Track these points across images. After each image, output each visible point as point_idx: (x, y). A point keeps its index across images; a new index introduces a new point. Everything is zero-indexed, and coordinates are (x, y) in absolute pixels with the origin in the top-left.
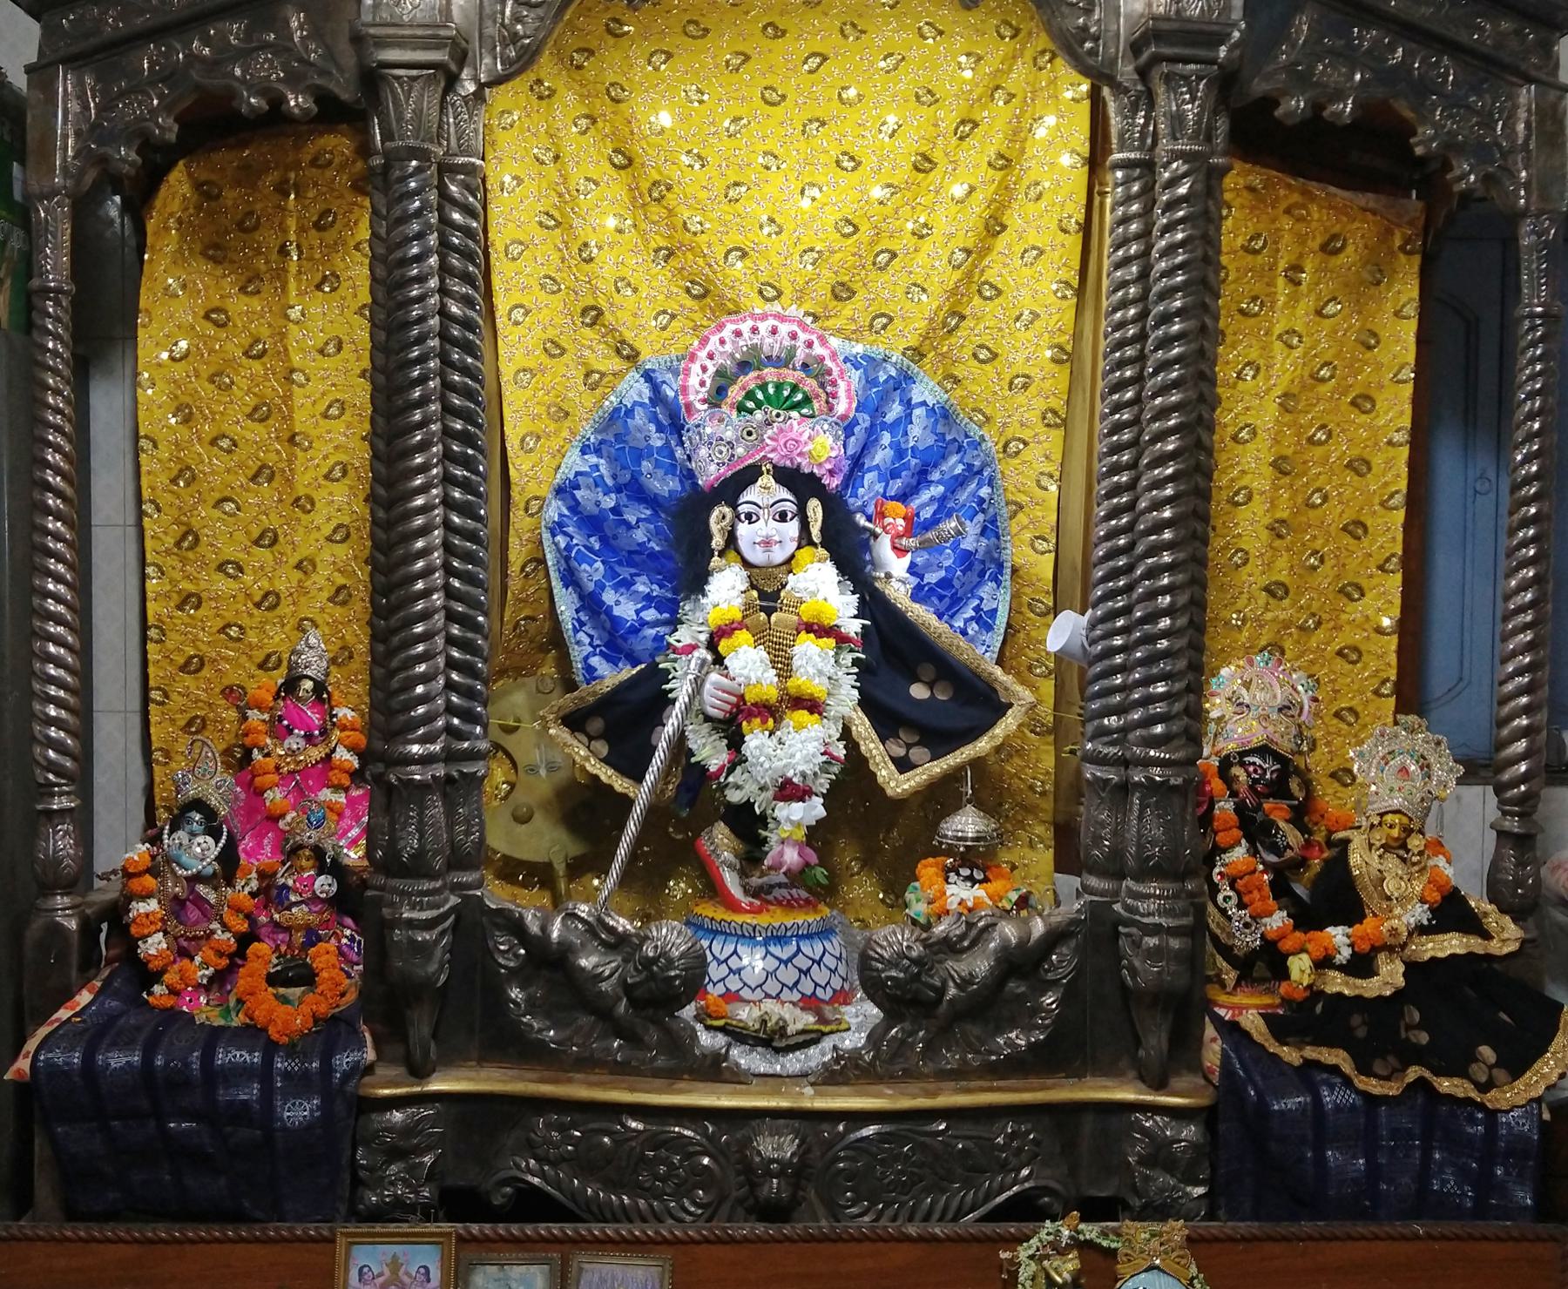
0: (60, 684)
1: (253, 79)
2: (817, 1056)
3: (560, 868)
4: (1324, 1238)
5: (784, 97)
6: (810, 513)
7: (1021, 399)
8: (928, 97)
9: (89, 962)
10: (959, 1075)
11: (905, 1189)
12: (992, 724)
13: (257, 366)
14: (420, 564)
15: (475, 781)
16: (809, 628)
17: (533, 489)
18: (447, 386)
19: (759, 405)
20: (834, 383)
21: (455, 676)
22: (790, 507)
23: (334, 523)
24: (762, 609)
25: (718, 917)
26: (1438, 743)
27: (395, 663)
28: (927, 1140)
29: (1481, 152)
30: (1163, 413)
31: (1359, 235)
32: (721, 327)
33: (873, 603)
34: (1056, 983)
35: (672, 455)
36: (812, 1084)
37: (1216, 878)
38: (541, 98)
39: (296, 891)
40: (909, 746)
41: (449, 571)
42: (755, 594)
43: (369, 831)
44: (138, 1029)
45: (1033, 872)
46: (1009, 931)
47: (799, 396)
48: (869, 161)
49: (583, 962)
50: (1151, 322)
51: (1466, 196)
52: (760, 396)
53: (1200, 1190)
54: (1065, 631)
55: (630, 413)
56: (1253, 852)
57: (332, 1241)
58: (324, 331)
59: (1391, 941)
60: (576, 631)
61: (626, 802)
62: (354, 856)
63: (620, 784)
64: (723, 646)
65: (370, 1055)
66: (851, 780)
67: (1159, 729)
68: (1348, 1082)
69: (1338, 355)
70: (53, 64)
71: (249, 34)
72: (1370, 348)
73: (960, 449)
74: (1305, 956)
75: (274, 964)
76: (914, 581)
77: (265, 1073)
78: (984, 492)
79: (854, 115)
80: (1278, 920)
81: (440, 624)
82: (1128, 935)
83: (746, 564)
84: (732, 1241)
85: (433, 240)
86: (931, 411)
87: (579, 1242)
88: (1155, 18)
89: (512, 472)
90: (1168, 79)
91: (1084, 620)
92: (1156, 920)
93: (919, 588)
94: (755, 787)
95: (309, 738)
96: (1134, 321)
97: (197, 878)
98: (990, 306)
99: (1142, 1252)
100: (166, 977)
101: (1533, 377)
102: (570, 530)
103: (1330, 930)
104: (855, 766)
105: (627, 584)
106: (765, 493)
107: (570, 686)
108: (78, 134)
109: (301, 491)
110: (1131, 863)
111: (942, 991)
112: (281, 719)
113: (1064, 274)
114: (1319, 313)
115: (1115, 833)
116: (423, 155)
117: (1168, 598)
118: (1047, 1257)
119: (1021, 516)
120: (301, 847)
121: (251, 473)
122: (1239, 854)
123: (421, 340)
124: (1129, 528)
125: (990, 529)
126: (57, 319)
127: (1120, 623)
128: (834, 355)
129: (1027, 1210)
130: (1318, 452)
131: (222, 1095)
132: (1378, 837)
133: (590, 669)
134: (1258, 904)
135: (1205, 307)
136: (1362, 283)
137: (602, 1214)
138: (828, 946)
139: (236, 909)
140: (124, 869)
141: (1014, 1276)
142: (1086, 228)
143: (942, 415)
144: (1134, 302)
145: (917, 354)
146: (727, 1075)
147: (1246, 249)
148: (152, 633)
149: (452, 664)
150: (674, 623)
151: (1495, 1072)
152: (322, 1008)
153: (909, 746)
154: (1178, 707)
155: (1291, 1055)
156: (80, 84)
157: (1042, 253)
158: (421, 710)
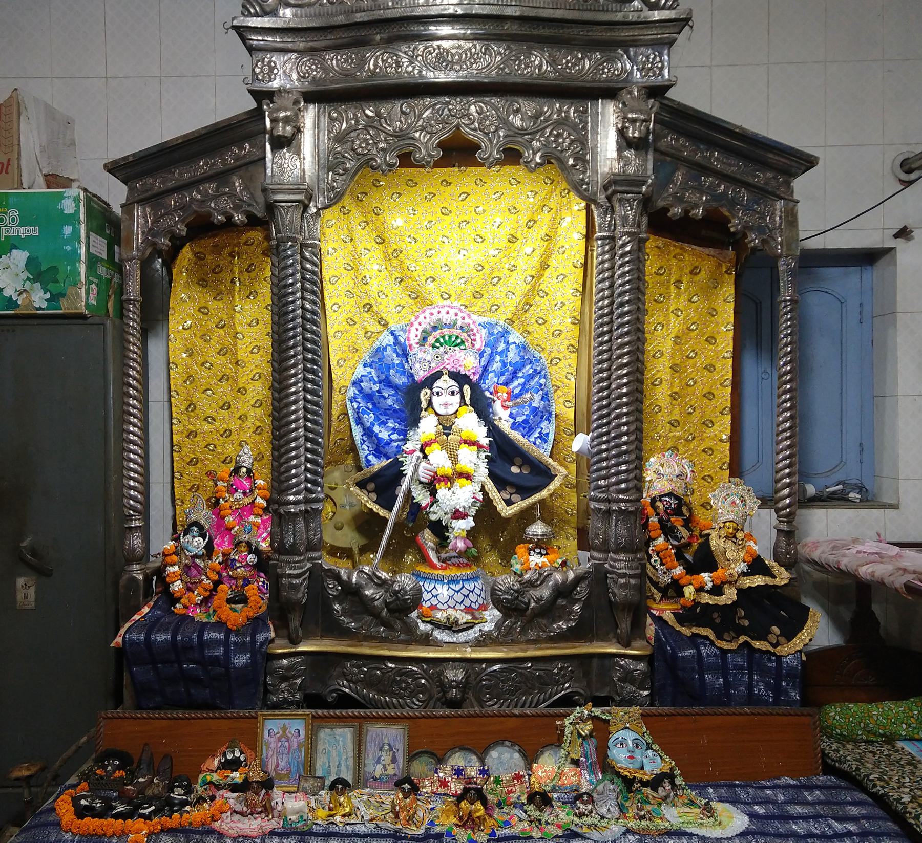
0: (135, 472)
2: (472, 634)
3: (356, 550)
6: (465, 391)
7: (558, 340)
8: (514, 210)
9: (148, 594)
11: (513, 693)
12: (548, 484)
13: (221, 331)
14: (294, 416)
15: (317, 512)
16: (465, 442)
17: (342, 383)
18: (305, 339)
20: (474, 335)
21: (309, 465)
22: (456, 389)
23: (255, 399)
24: (444, 434)
25: (427, 571)
27: (282, 460)
29: (760, 230)
30: (622, 346)
31: (707, 266)
32: (424, 311)
33: (493, 430)
35: (404, 368)
37: (651, 552)
40: (511, 494)
41: (306, 419)
43: (271, 534)
44: (169, 623)
46: (558, 577)
47: (459, 341)
49: (367, 593)
51: (754, 249)
52: (442, 340)
53: (646, 693)
54: (580, 442)
55: (385, 349)
56: (667, 540)
57: (256, 718)
60: (362, 444)
61: (385, 521)
62: (264, 546)
64: (427, 450)
65: (273, 635)
66: (485, 511)
67: (623, 486)
68: (712, 643)
70: (134, 203)
71: (217, 190)
72: (713, 316)
74: (691, 586)
76: (512, 421)
78: (542, 381)
79: (481, 218)
80: (679, 571)
81: (302, 442)
83: (437, 414)
84: (436, 717)
85: (298, 276)
87: (367, 718)
89: (333, 375)
90: (620, 200)
91: (589, 437)
92: (624, 571)
93: (514, 424)
94: (442, 513)
95: (244, 494)
97: (196, 556)
98: (543, 300)
102: (359, 400)
104: (487, 502)
105: (384, 423)
106: (445, 383)
107: (360, 469)
108: (143, 233)
110: (612, 546)
111: (528, 604)
112: (232, 485)
113: (576, 286)
114: (690, 301)
115: (605, 532)
116: (294, 240)
117: (626, 428)
118: (578, 723)
119: (558, 391)
120: (241, 542)
121: (219, 378)
122: (661, 540)
123: (293, 320)
124: (608, 396)
125: (545, 397)
126: (135, 313)
127: (605, 439)
128: (474, 322)
129: (568, 702)
130: (691, 361)
132: (723, 533)
133: (368, 461)
137: (376, 705)
139: (213, 570)
140: (163, 553)
141: (563, 732)
142: (585, 266)
143: (523, 348)
144: (608, 297)
145: (511, 321)
146: (432, 643)
147: (657, 274)
149: (307, 460)
150: (405, 440)
152: (251, 614)
153: (511, 494)
155: (686, 631)
156: (144, 211)
158: (294, 480)
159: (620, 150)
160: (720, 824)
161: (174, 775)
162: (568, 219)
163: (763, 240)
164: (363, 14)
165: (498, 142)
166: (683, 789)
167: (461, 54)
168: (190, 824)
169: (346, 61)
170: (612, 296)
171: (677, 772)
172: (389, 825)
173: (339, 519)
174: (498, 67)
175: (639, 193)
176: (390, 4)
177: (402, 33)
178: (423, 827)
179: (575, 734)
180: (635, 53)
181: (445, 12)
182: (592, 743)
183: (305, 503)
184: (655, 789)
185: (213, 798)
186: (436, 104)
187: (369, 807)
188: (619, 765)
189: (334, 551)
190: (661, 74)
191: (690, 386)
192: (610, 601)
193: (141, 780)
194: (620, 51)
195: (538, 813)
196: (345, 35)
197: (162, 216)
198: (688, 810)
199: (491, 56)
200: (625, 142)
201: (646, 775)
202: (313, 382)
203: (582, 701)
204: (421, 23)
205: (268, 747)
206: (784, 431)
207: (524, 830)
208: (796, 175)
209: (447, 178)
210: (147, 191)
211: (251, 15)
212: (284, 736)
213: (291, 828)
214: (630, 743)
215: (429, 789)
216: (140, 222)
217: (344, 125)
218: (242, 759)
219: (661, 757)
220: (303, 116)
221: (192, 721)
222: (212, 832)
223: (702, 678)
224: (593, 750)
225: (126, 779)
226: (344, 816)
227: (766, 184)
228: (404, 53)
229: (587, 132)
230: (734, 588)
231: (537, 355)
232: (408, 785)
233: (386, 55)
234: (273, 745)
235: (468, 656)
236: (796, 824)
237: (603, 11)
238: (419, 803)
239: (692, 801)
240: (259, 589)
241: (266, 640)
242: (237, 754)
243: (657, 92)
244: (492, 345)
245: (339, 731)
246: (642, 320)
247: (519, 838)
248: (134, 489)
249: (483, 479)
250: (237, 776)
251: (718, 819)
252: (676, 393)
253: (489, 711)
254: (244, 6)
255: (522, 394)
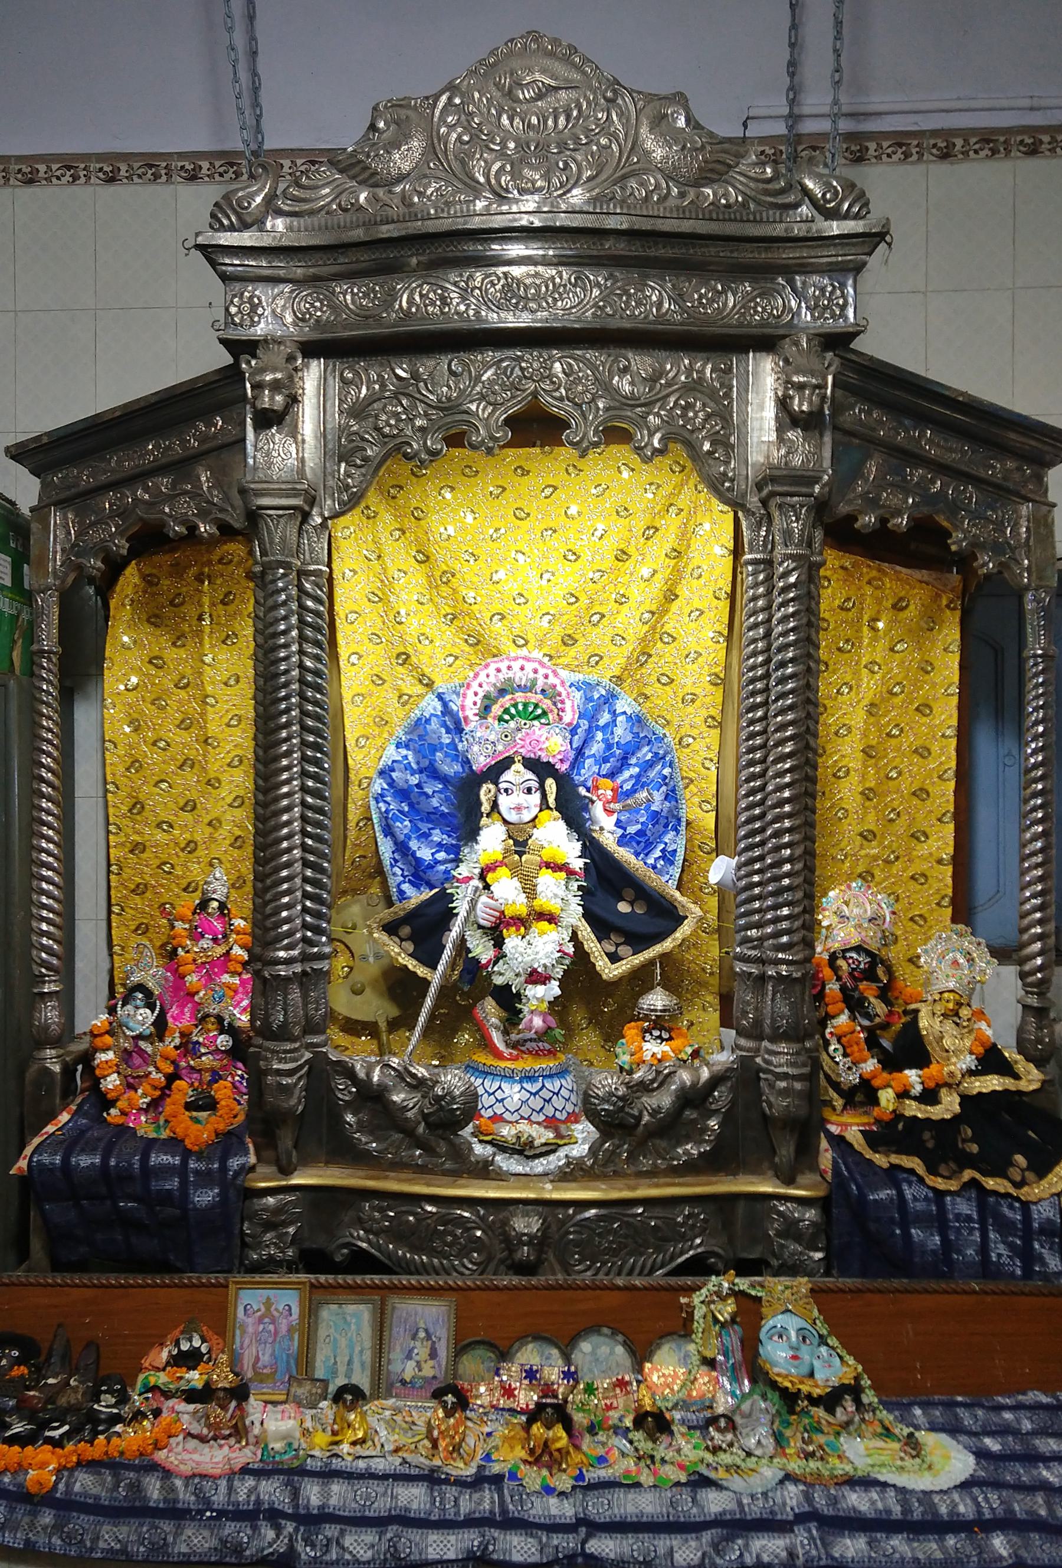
0: (50, 909)
1: (175, 516)
2: (555, 1161)
3: (383, 1026)
4: (907, 1291)
5: (528, 514)
6: (547, 789)
7: (690, 709)
8: (623, 511)
9: (68, 1091)
10: (652, 1174)
11: (615, 1253)
12: (674, 930)
13: (183, 694)
14: (285, 831)
15: (324, 976)
16: (548, 865)
17: (364, 772)
18: (304, 713)
19: (512, 717)
20: (562, 702)
21: (308, 904)
22: (534, 785)
23: (233, 795)
24: (516, 852)
25: (488, 1063)
26: (979, 944)
27: (268, 896)
28: (631, 1220)
29: (997, 548)
30: (782, 727)
31: (917, 599)
32: (487, 666)
33: (591, 848)
34: (717, 1111)
35: (456, 750)
36: (552, 1181)
37: (828, 1036)
38: (368, 518)
39: (204, 1045)
40: (617, 945)
41: (304, 833)
42: (511, 842)
43: (252, 1005)
44: (99, 1140)
45: (706, 1027)
46: (685, 1076)
47: (539, 711)
48: (586, 555)
49: (395, 1098)
50: (772, 666)
51: (988, 577)
52: (513, 711)
53: (818, 1255)
54: (720, 869)
55: (428, 721)
56: (853, 1018)
57: (227, 1287)
58: (226, 671)
59: (950, 1081)
60: (392, 866)
61: (426, 983)
62: (244, 1019)
63: (421, 971)
64: (490, 878)
65: (252, 1159)
66: (578, 970)
67: (785, 939)
68: (921, 1180)
69: (906, 677)
70: (48, 506)
71: (174, 485)
72: (928, 673)
73: (649, 742)
74: (890, 1090)
75: (190, 1095)
76: (620, 832)
77: (182, 1171)
78: (666, 771)
79: (575, 525)
80: (871, 1065)
81: (299, 870)
82: (766, 1080)
83: (505, 822)
84: (497, 1288)
85: (294, 620)
86: (629, 718)
87: (393, 1288)
88: (772, 467)
89: (350, 761)
90: (780, 506)
91: (734, 862)
92: (785, 1069)
93: (623, 836)
94: (512, 974)
95: (215, 940)
96: (761, 665)
97: (140, 1037)
98: (668, 648)
99: (779, 1299)
100: (119, 1104)
101: (1037, 697)
102: (388, 799)
103: (907, 1072)
104: (581, 955)
105: (426, 836)
106: (517, 775)
107: (390, 904)
108: (63, 550)
109: (212, 775)
110: (767, 1030)
112: (196, 927)
113: (718, 627)
114: (892, 650)
115: (756, 1009)
116: (287, 566)
117: (788, 851)
118: (713, 1302)
119: (692, 786)
120: (208, 1016)
121: (178, 764)
122: (843, 1019)
123: (286, 685)
124: (762, 803)
125: (671, 796)
126: (49, 671)
127: (757, 866)
128: (563, 683)
129: (700, 1267)
130: (893, 741)
131: (154, 1185)
132: (939, 1009)
133: (401, 892)
134: (857, 1054)
135: (809, 656)
136: (922, 629)
137: (409, 1268)
138: (564, 1082)
139: (166, 1058)
140: (91, 1032)
141: (691, 1315)
142: (732, 597)
143: (637, 720)
144: (762, 652)
145: (619, 679)
146: (493, 1175)
147: (842, 608)
148: (114, 868)
149: (306, 895)
150: (457, 861)
151: (1027, 1173)
152: (221, 1127)
153: (617, 945)
154: (797, 924)
155: (880, 1160)
156: (65, 518)
157: (702, 613)
158: (285, 928)
159: (780, 430)
160: (930, 1467)
161: (102, 1373)
162: (707, 526)
163: (1001, 564)
164: (391, 227)
165: (596, 417)
166: (874, 1411)
167: (539, 286)
168: (122, 1453)
169: (366, 295)
170: (768, 649)
171: (866, 1382)
172: (422, 1460)
173: (358, 977)
174: (596, 305)
175: (811, 495)
176: (432, 211)
177: (450, 255)
178: (474, 1464)
179: (710, 1318)
180: (804, 283)
181: (516, 224)
182: (735, 1331)
183: (302, 961)
184: (831, 1411)
185: (157, 1413)
186: (502, 360)
187: (393, 1430)
188: (776, 1370)
189: (353, 1027)
190: (843, 315)
191: (891, 779)
192: (764, 1114)
193: (51, 1381)
194: (780, 280)
195: (650, 1445)
196: (366, 257)
197: (92, 525)
198: (880, 1444)
199: (584, 290)
200: (788, 418)
201: (817, 1386)
202: (315, 777)
203: (721, 1266)
204: (478, 240)
205: (244, 1332)
206: (1034, 854)
207: (627, 1472)
208: (1051, 464)
209: (523, 464)
210: (69, 488)
211: (223, 228)
212: (268, 1314)
213: (274, 1462)
214: (793, 1334)
215: (485, 1400)
216: (58, 533)
217: (364, 391)
218: (204, 1350)
219: (841, 1358)
220: (302, 379)
221: (131, 1290)
222: (154, 1467)
223: (907, 1235)
224: (737, 1344)
225: (30, 1379)
226: (354, 1443)
227: (1004, 478)
228: (452, 283)
229: (731, 403)
230: (955, 1095)
231: (660, 731)
232: (453, 1396)
233: (426, 287)
234: (250, 1329)
235: (547, 1196)
236: (1048, 1468)
237: (755, 221)
238: (469, 1424)
239: (887, 1429)
240: (235, 1087)
241: (242, 1167)
242: (197, 1343)
243: (837, 342)
244: (590, 716)
245: (351, 1308)
246: (814, 686)
247: (620, 1485)
248: (48, 935)
249: (573, 921)
250: (195, 1378)
251: (928, 1459)
252: (870, 789)
253: (578, 1279)
254: (213, 216)
255: (635, 791)
